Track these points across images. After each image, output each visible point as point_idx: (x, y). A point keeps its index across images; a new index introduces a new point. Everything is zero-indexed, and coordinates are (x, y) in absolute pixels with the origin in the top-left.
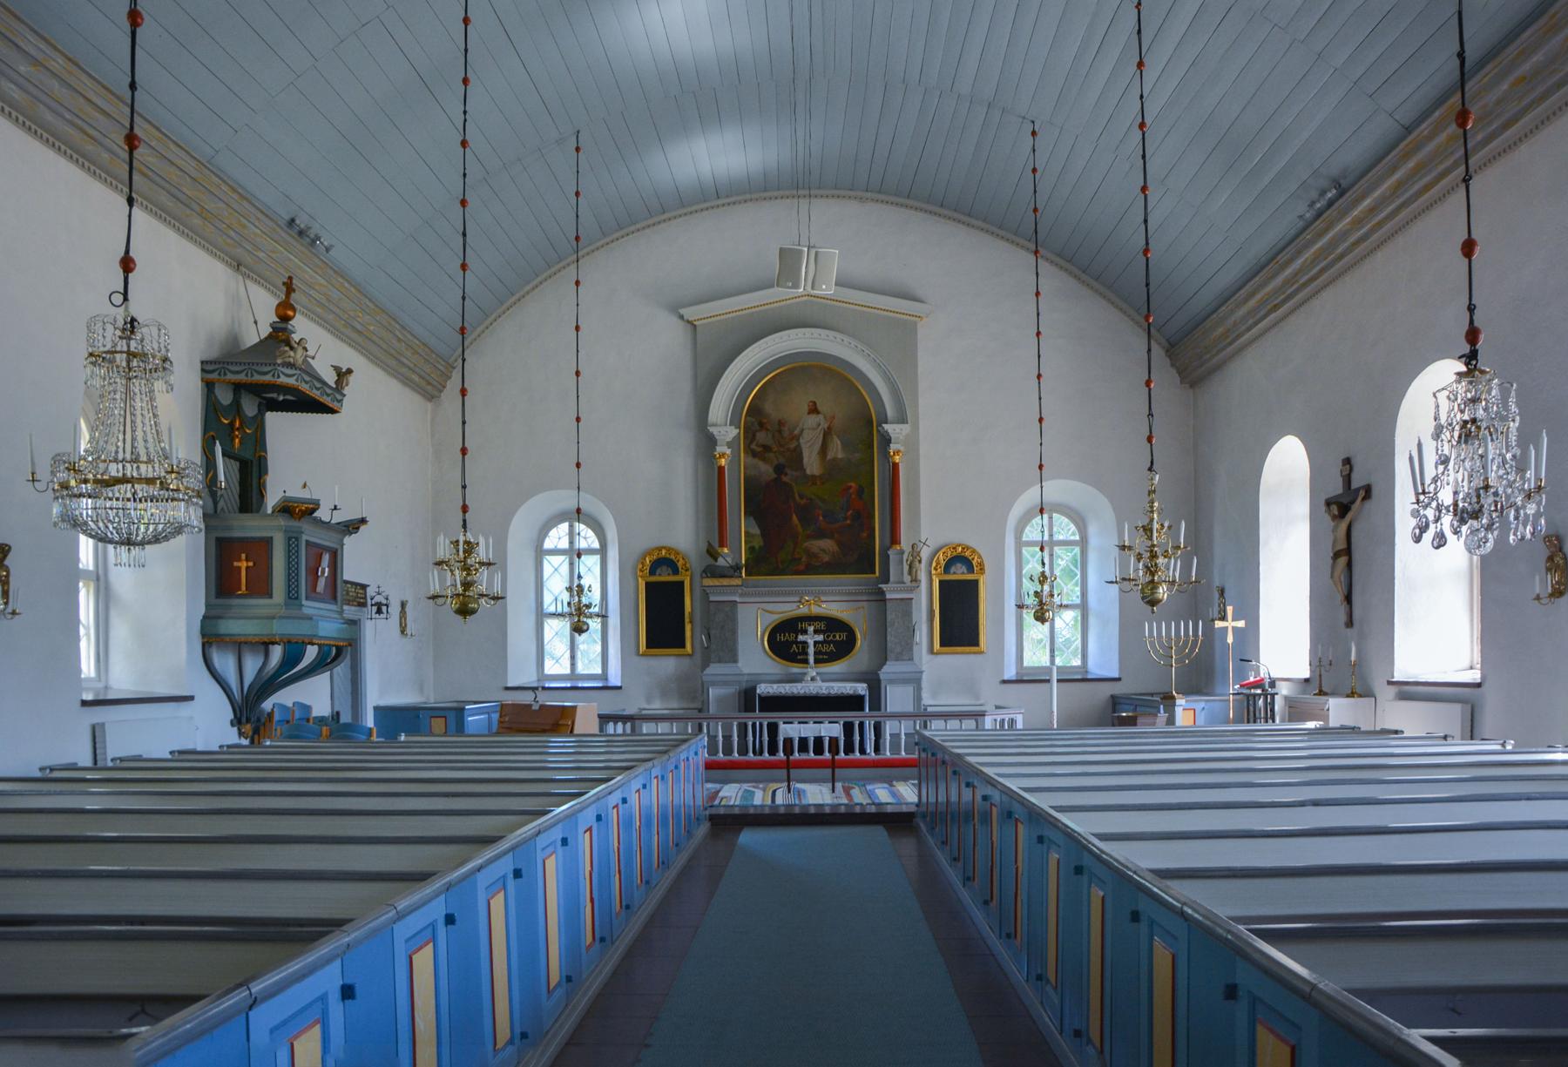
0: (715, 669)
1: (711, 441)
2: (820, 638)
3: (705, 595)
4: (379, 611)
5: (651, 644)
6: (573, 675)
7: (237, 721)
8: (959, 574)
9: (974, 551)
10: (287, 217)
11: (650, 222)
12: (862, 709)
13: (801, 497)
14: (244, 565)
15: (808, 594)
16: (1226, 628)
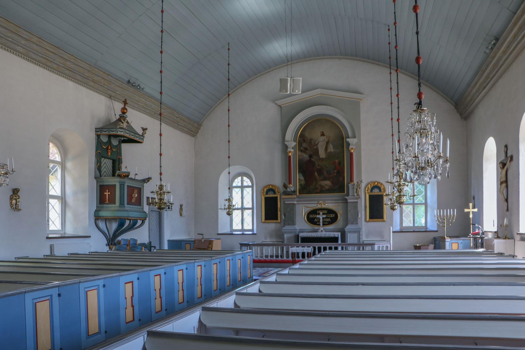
0: (287, 228)
1: (286, 147)
2: (325, 216)
3: (284, 202)
4: (169, 208)
5: (266, 219)
6: (243, 230)
7: (108, 245)
8: (376, 192)
9: (381, 184)
10: (127, 80)
11: (266, 71)
12: (337, 242)
13: (318, 166)
14: (107, 193)
15: (320, 200)
16: (469, 212)
